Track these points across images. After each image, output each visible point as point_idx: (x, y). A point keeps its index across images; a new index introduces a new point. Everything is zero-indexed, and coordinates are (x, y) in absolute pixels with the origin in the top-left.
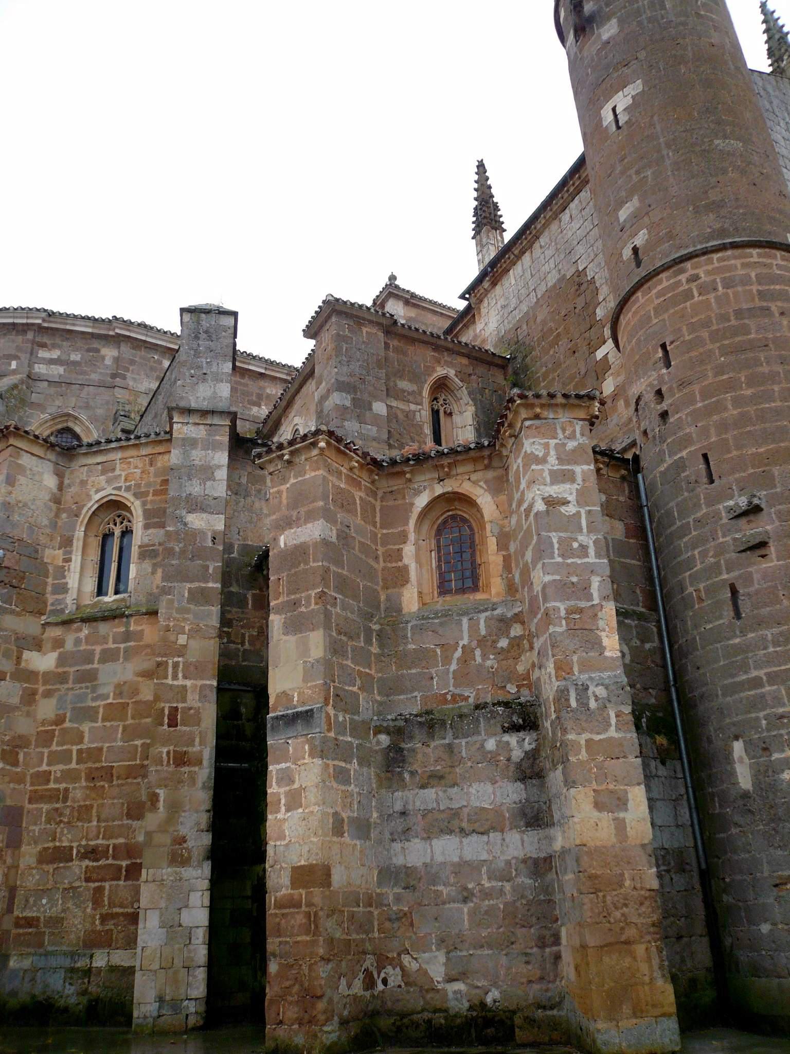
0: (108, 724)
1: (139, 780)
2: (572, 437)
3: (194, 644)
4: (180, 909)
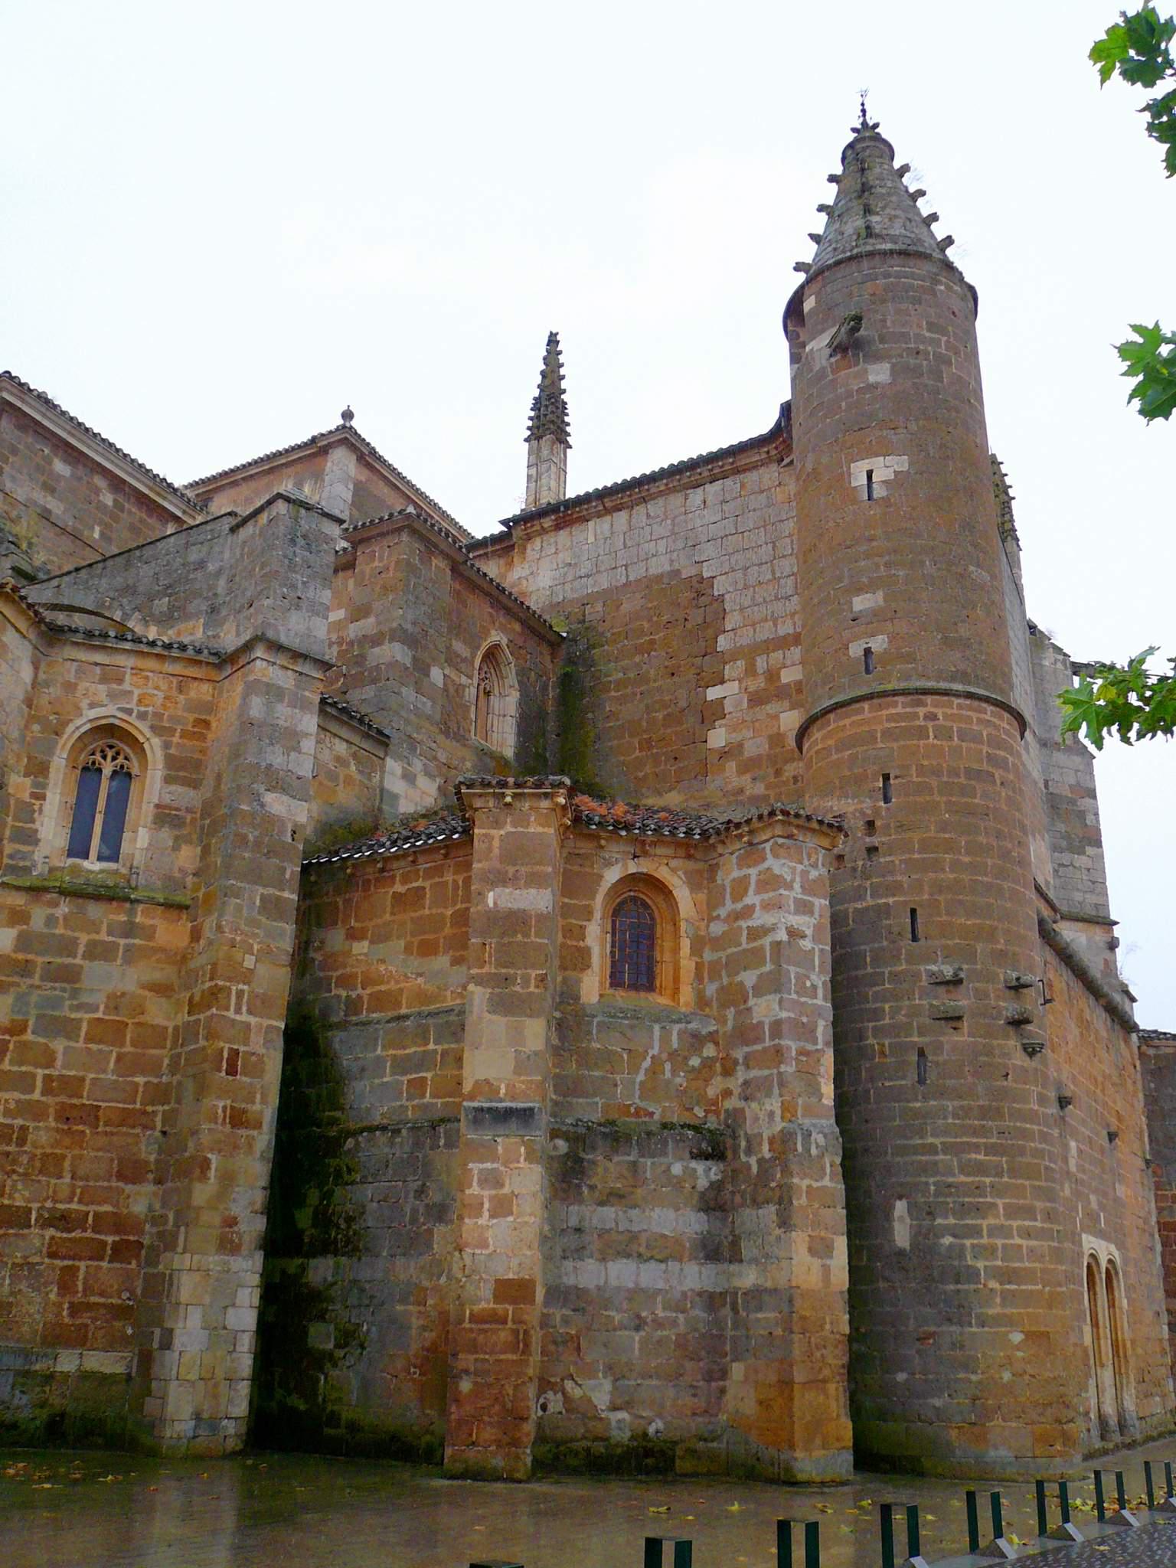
0: (94, 1047)
1: (138, 1130)
2: (815, 866)
3: (262, 970)
4: (226, 1308)
